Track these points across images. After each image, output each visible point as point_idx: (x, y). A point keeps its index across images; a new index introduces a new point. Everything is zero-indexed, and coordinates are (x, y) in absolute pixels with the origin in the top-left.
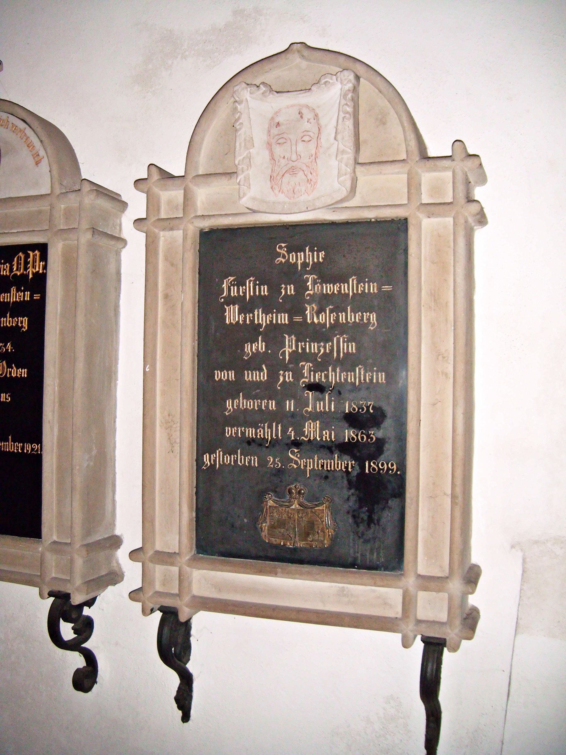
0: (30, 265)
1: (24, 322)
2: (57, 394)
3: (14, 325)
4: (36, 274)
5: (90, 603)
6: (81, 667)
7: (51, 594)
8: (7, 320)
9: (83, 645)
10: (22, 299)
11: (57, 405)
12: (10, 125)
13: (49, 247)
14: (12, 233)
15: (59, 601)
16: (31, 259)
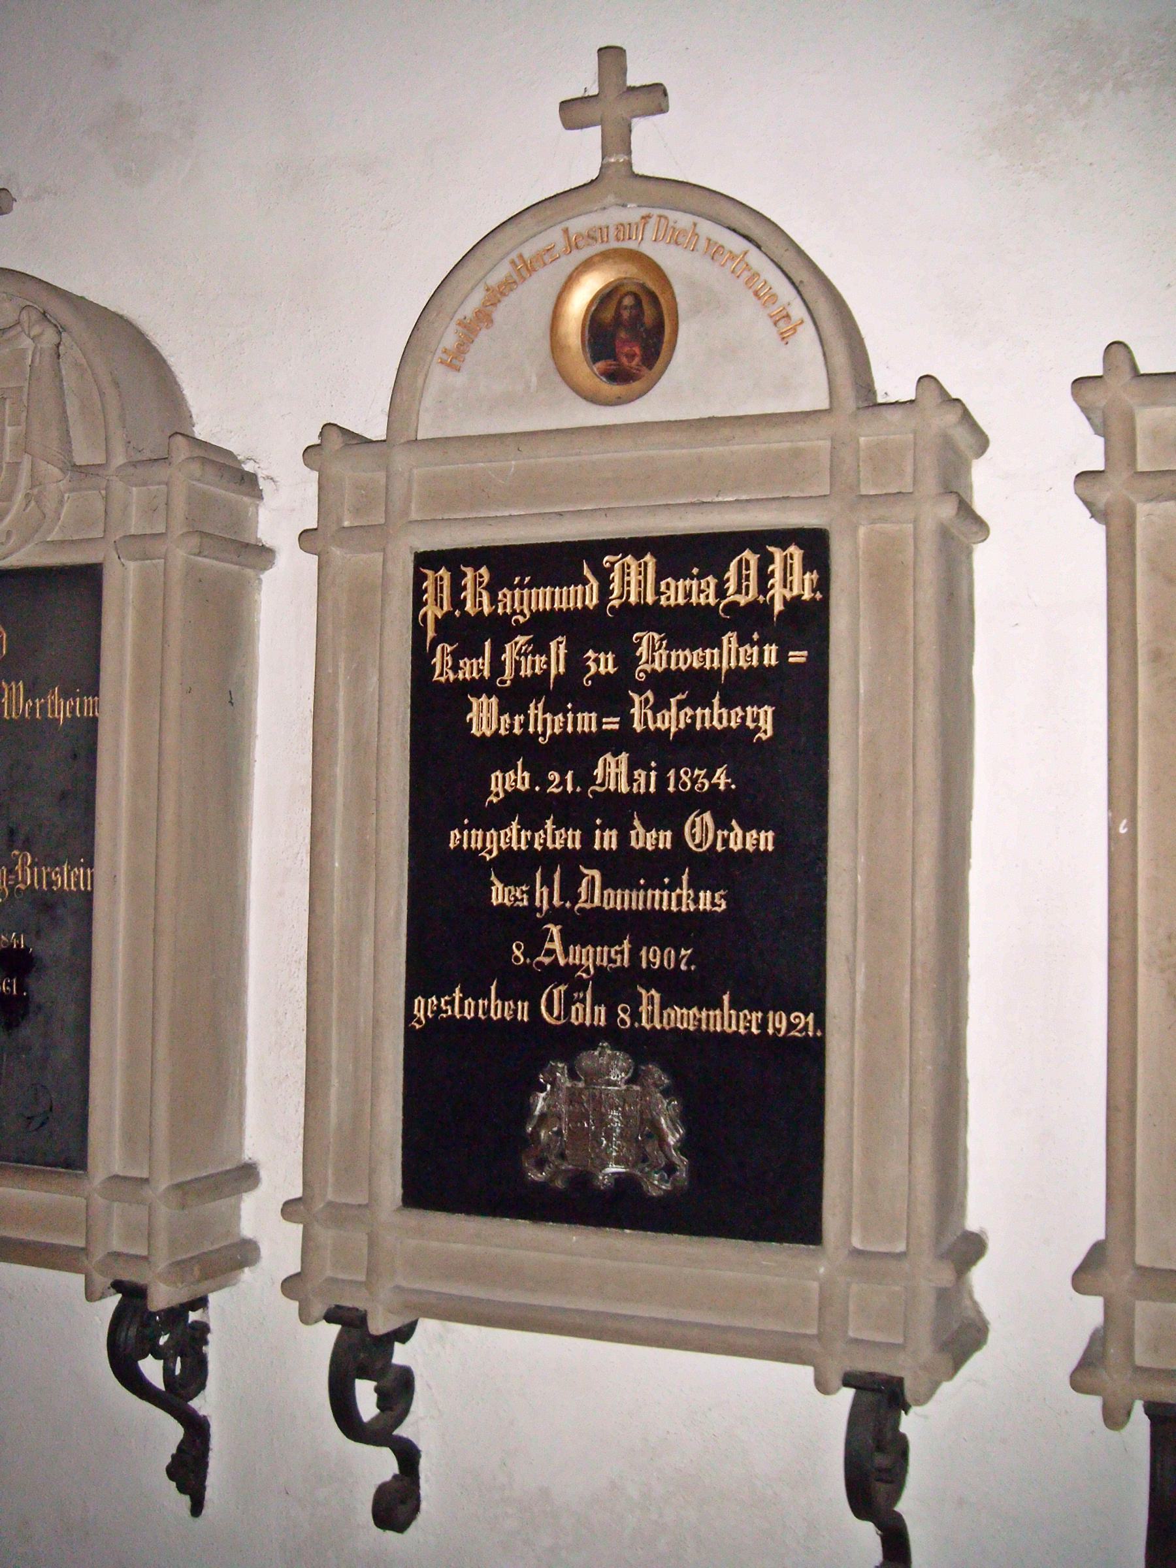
0: (777, 580)
1: (763, 720)
2: (861, 891)
3: (733, 724)
4: (794, 604)
5: (404, 1334)
6: (388, 1477)
7: (330, 1318)
8: (712, 714)
9: (396, 1433)
10: (755, 663)
11: (862, 918)
12: (703, 243)
13: (105, 571)
14: (719, 503)
15: (869, 1397)
16: (777, 567)
